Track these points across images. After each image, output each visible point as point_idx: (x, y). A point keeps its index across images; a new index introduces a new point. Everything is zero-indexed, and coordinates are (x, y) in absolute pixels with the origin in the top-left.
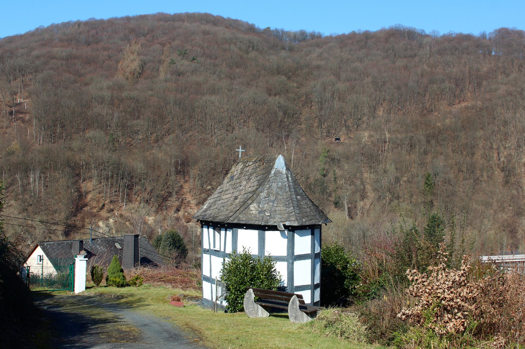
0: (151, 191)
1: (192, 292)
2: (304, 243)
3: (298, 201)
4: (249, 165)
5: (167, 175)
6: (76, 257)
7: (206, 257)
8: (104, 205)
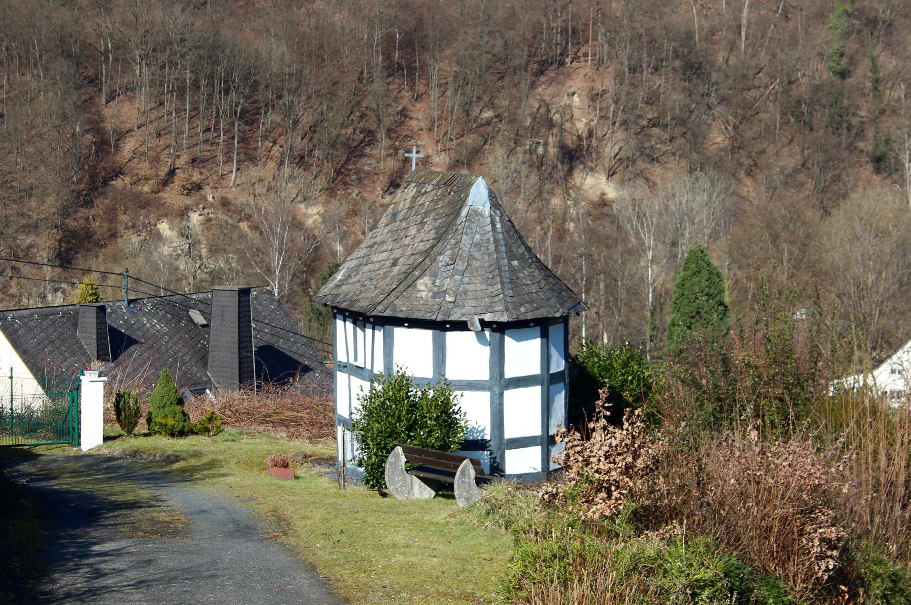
0: (313, 128)
1: (321, 449)
2: (524, 355)
3: (513, 270)
4: (426, 192)
5: (360, 79)
6: (84, 375)
7: (342, 378)
8: (172, 172)
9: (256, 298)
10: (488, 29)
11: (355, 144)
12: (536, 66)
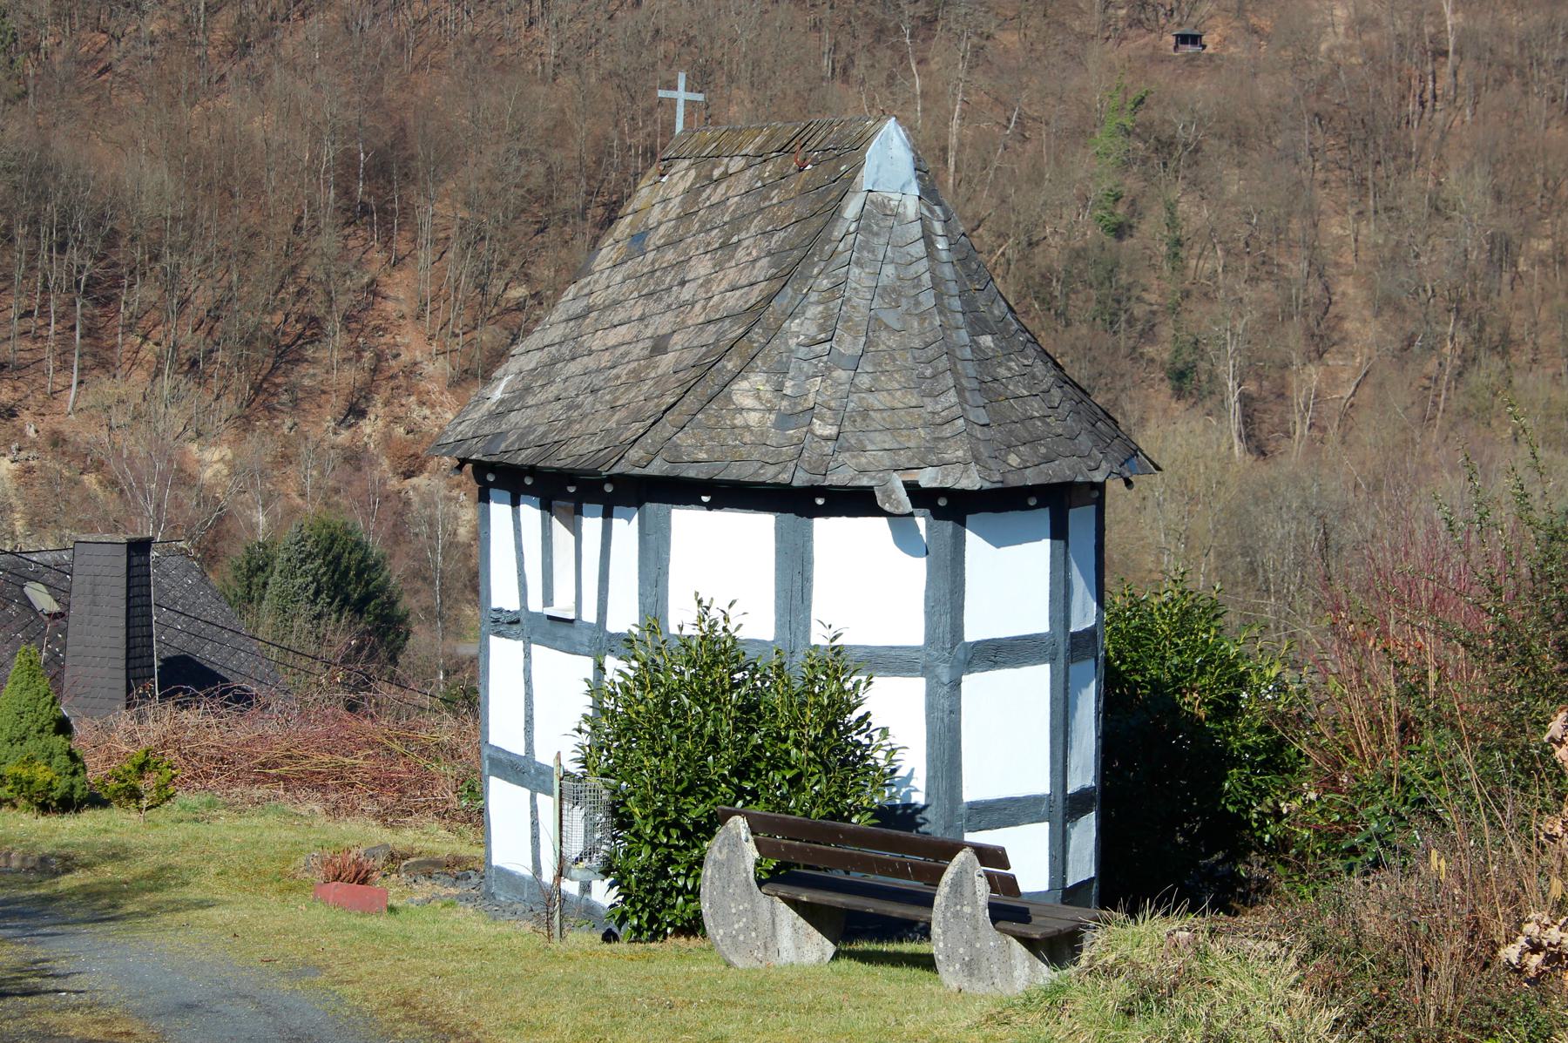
0: (215, 314)
1: (430, 837)
2: (1012, 581)
3: (982, 359)
4: (726, 175)
5: (297, 229)
9: (158, 564)
10: (519, 146)
11: (288, 340)
12: (600, 211)
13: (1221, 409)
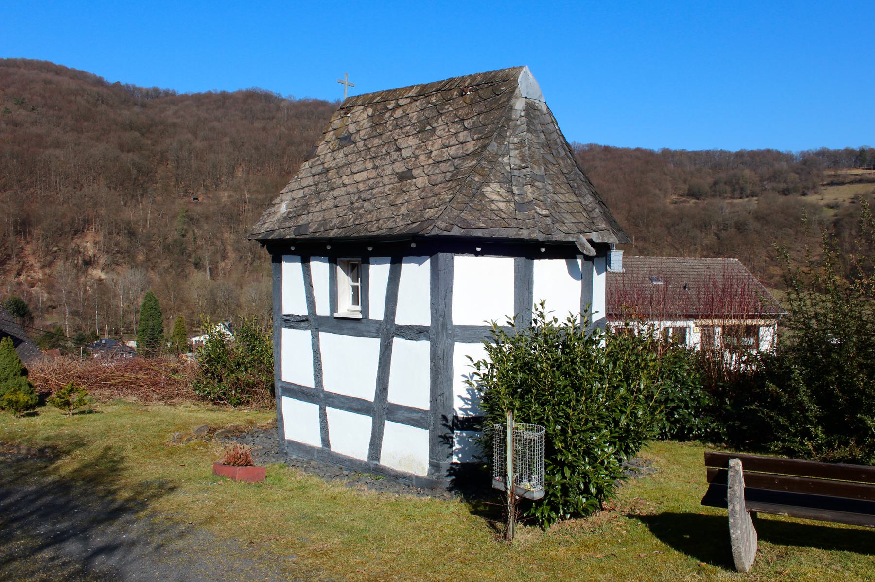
13: (205, 271)
